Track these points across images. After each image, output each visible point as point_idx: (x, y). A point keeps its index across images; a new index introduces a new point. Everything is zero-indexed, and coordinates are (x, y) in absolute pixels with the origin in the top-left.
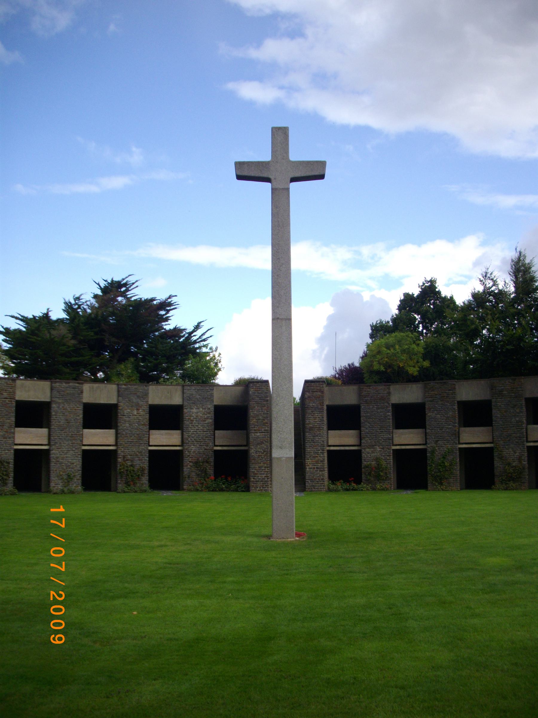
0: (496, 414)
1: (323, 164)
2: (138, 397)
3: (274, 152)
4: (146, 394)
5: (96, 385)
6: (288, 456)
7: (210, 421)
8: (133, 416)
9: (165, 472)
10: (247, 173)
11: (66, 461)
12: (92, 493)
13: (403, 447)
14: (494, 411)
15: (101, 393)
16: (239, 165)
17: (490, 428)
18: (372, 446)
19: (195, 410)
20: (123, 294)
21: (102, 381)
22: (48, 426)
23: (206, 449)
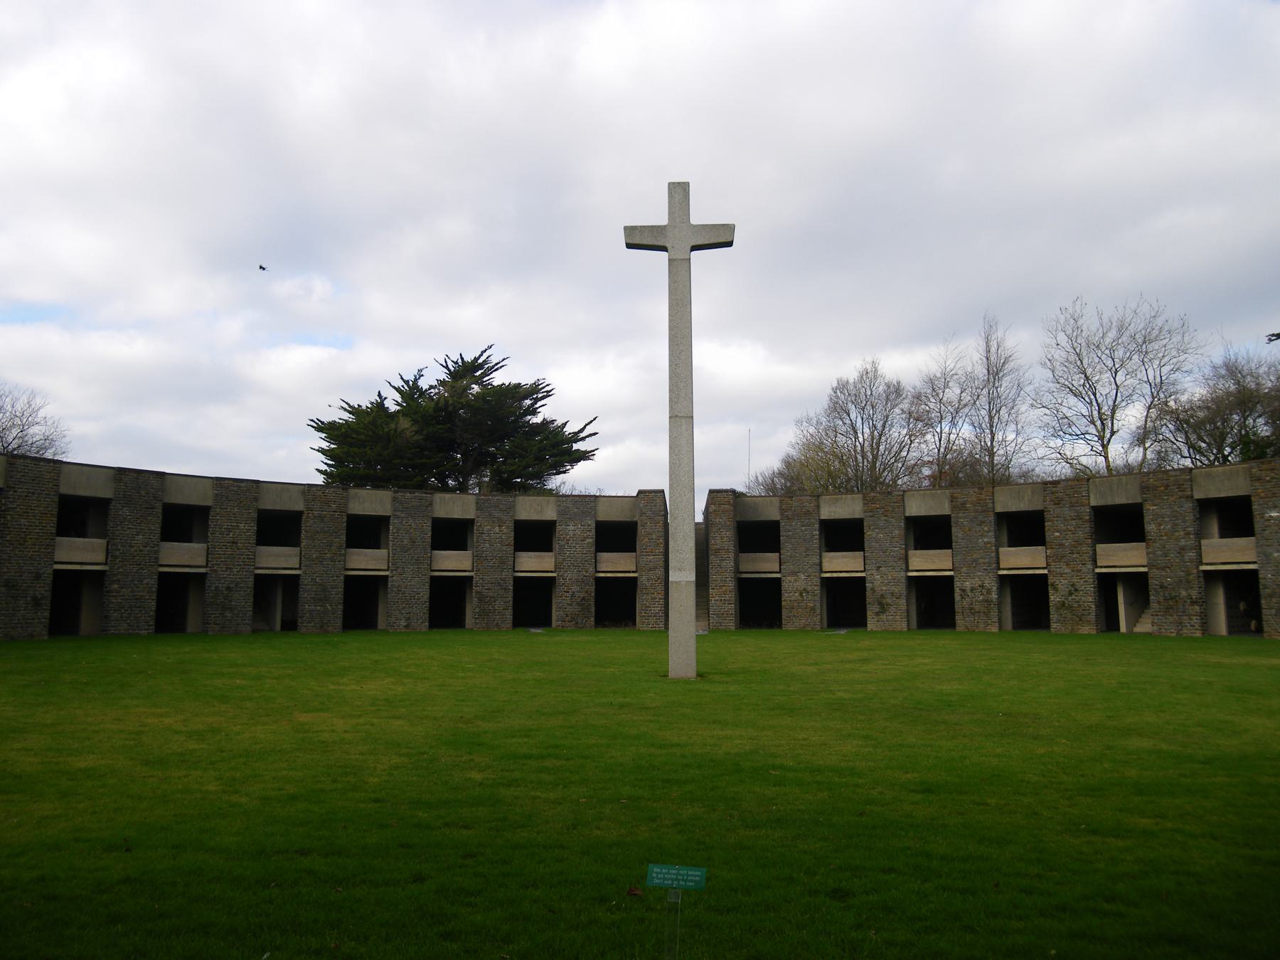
0: (957, 533)
1: (730, 228)
2: (501, 510)
4: (512, 507)
5: (448, 496)
8: (410, 529)
9: (532, 603)
10: (639, 240)
11: (409, 593)
12: (754, 632)
13: (835, 575)
14: (954, 530)
15: (453, 506)
16: (629, 230)
17: (64, 490)
18: (794, 573)
19: (571, 528)
20: (479, 381)
21: (452, 490)
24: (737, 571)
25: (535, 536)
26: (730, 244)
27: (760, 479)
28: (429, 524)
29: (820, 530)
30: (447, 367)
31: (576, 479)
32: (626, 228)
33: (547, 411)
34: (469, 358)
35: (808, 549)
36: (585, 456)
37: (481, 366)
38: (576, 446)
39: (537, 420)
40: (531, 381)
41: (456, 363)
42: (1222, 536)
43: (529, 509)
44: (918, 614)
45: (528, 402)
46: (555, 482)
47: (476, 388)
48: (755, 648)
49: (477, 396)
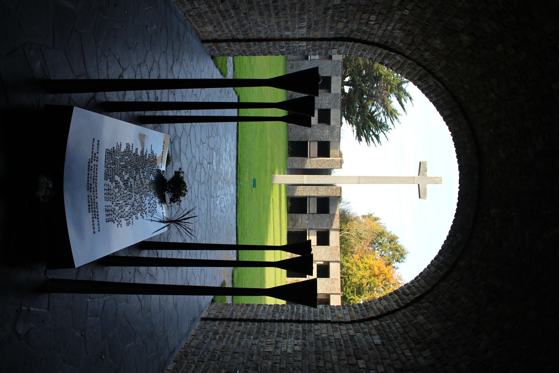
1: (425, 198)
3: (431, 178)
4: (336, 107)
10: (422, 167)
16: (425, 163)
18: (308, 219)
19: (327, 131)
24: (310, 197)
25: (325, 117)
26: (420, 198)
27: (124, 222)
28: (329, 75)
31: (347, 130)
43: (335, 114)
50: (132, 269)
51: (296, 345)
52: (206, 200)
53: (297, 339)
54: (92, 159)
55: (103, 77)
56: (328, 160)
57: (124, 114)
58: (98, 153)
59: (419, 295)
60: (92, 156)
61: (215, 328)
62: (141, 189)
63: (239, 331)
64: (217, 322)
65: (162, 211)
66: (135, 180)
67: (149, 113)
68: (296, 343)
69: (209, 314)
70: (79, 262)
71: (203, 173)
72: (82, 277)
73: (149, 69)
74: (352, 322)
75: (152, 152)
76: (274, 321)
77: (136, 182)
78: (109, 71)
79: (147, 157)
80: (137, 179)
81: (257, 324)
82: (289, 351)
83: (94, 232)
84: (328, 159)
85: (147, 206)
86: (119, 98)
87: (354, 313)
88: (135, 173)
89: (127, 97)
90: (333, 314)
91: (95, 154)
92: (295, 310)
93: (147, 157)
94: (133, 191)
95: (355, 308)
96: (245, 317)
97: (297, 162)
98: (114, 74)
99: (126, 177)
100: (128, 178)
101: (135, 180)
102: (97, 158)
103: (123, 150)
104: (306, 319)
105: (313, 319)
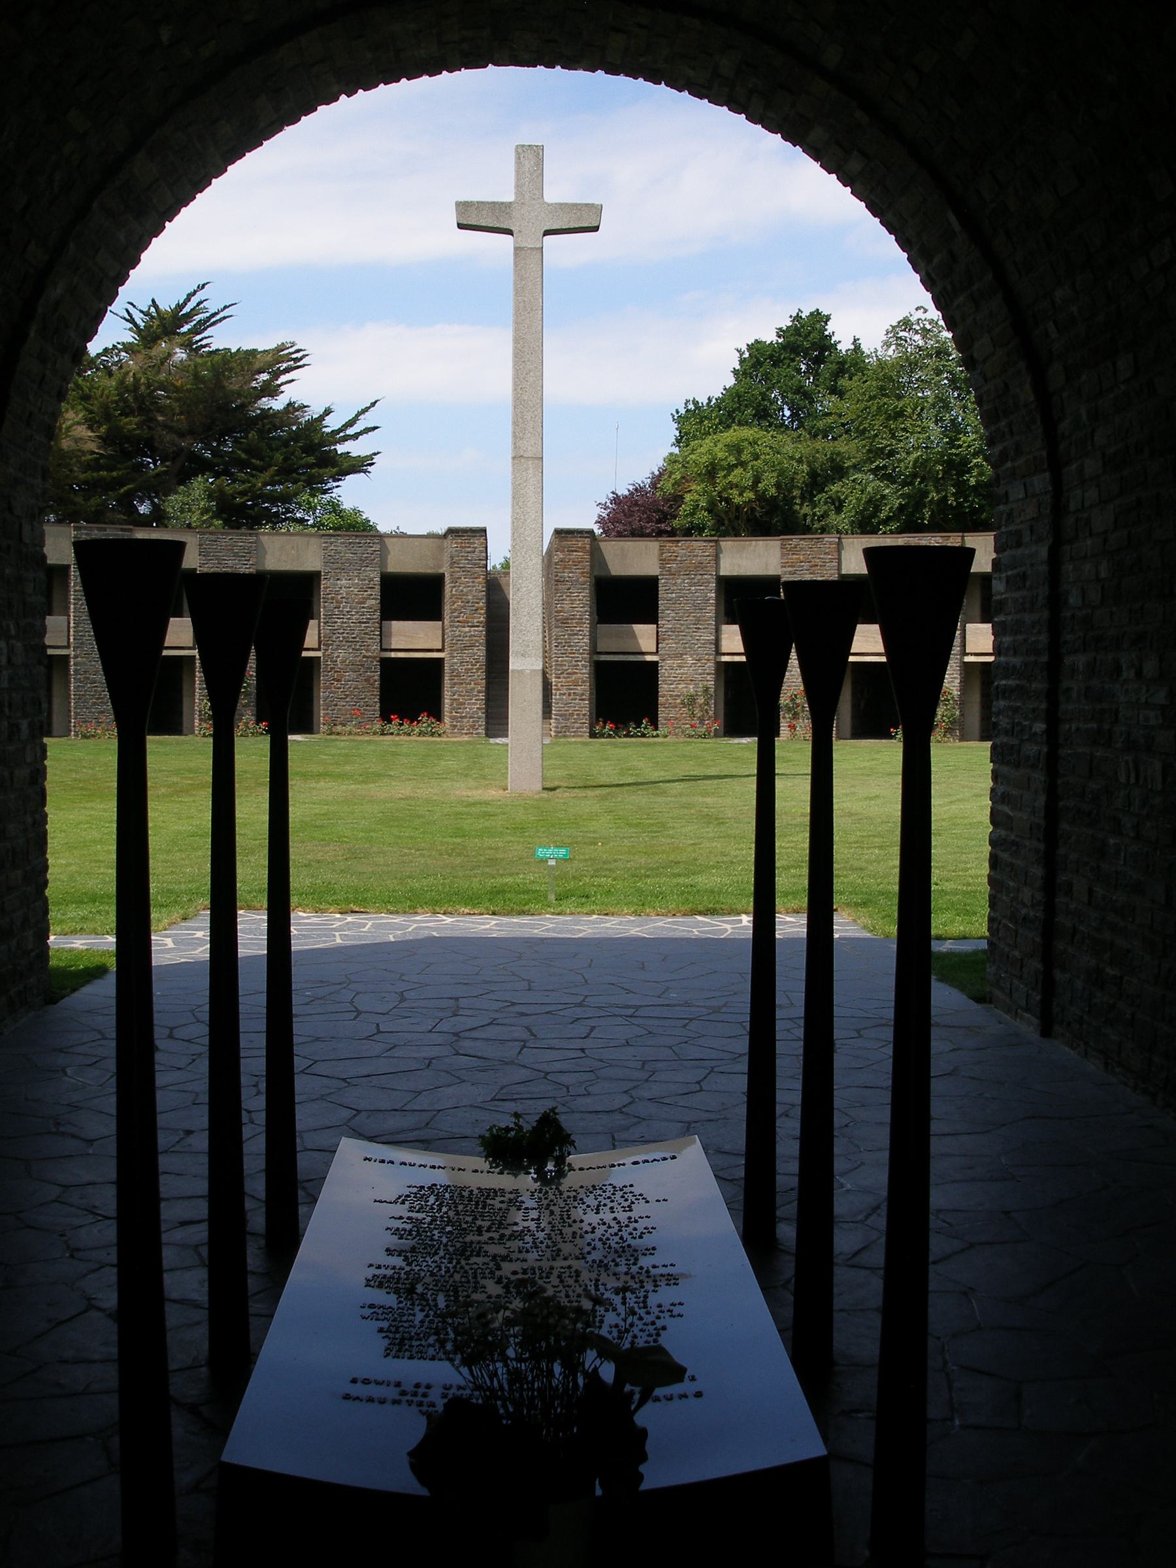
1: (598, 210)
2: (236, 555)
3: (518, 186)
6: (534, 668)
7: (373, 602)
10: (473, 218)
16: (463, 207)
22: (719, 664)
23: (365, 657)
24: (594, 651)
27: (663, 1296)
29: (718, 592)
30: (132, 320)
32: (458, 204)
33: (303, 391)
34: (167, 304)
35: (698, 620)
36: (360, 465)
37: (188, 317)
38: (341, 449)
39: (277, 404)
40: (271, 345)
41: (146, 314)
42: (507, 736)
44: (853, 717)
45: (264, 377)
46: (94, 347)
47: (180, 355)
48: (623, 754)
49: (182, 367)
50: (841, 1275)
51: (1139, 673)
52: (592, 1023)
53: (1117, 669)
54: (420, 1404)
55: (110, 1375)
56: (454, 581)
57: (254, 1307)
58: (398, 1384)
59: (952, 219)
60: (410, 1403)
61: (1079, 984)
62: (541, 1235)
63: (1091, 892)
64: (1059, 975)
65: (629, 1166)
66: (505, 1258)
67: (257, 1220)
68: (1132, 674)
69: (1027, 1010)
70: (804, 1442)
71: (491, 1032)
72: (862, 1438)
73: (91, 1218)
74: (1055, 466)
75: (402, 1200)
76: (1052, 763)
77: (514, 1256)
78: (97, 1357)
79: (420, 1216)
80: (504, 1252)
81: (1064, 826)
82: (1161, 697)
83: (699, 1395)
84: (447, 579)
85: (607, 1216)
86: (198, 1323)
87: (1021, 461)
88: (480, 1260)
89: (194, 1296)
90: (1027, 538)
91: (404, 1393)
92: (1011, 682)
93: (420, 1216)
94: (545, 1265)
95: (1004, 457)
96: (1038, 871)
97: (462, 692)
98: (99, 1338)
99: (494, 1289)
100: (499, 1281)
101: (505, 1258)
102: (417, 1386)
103: (391, 1300)
104: (1044, 638)
105: (1046, 614)
